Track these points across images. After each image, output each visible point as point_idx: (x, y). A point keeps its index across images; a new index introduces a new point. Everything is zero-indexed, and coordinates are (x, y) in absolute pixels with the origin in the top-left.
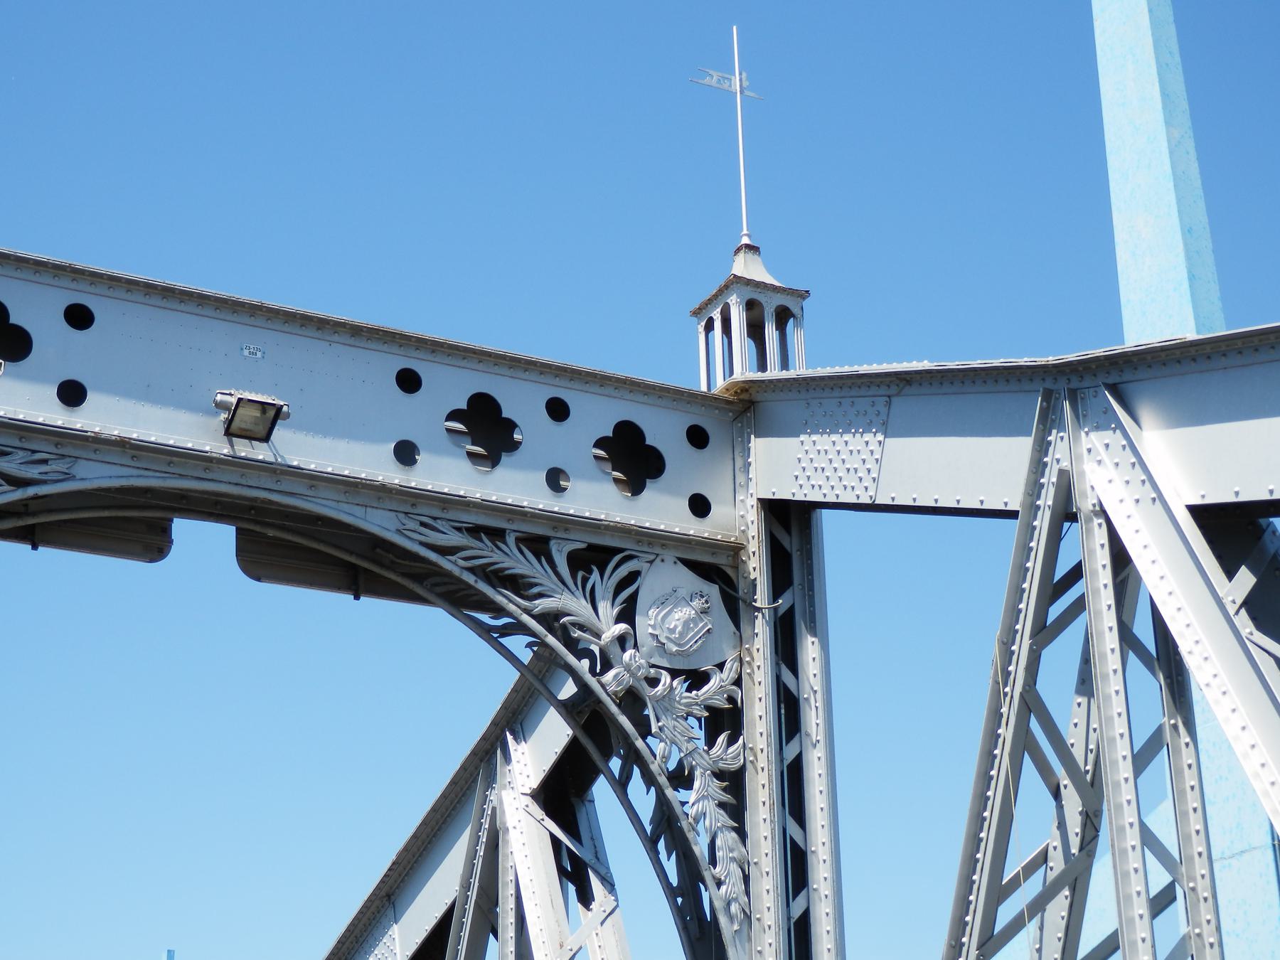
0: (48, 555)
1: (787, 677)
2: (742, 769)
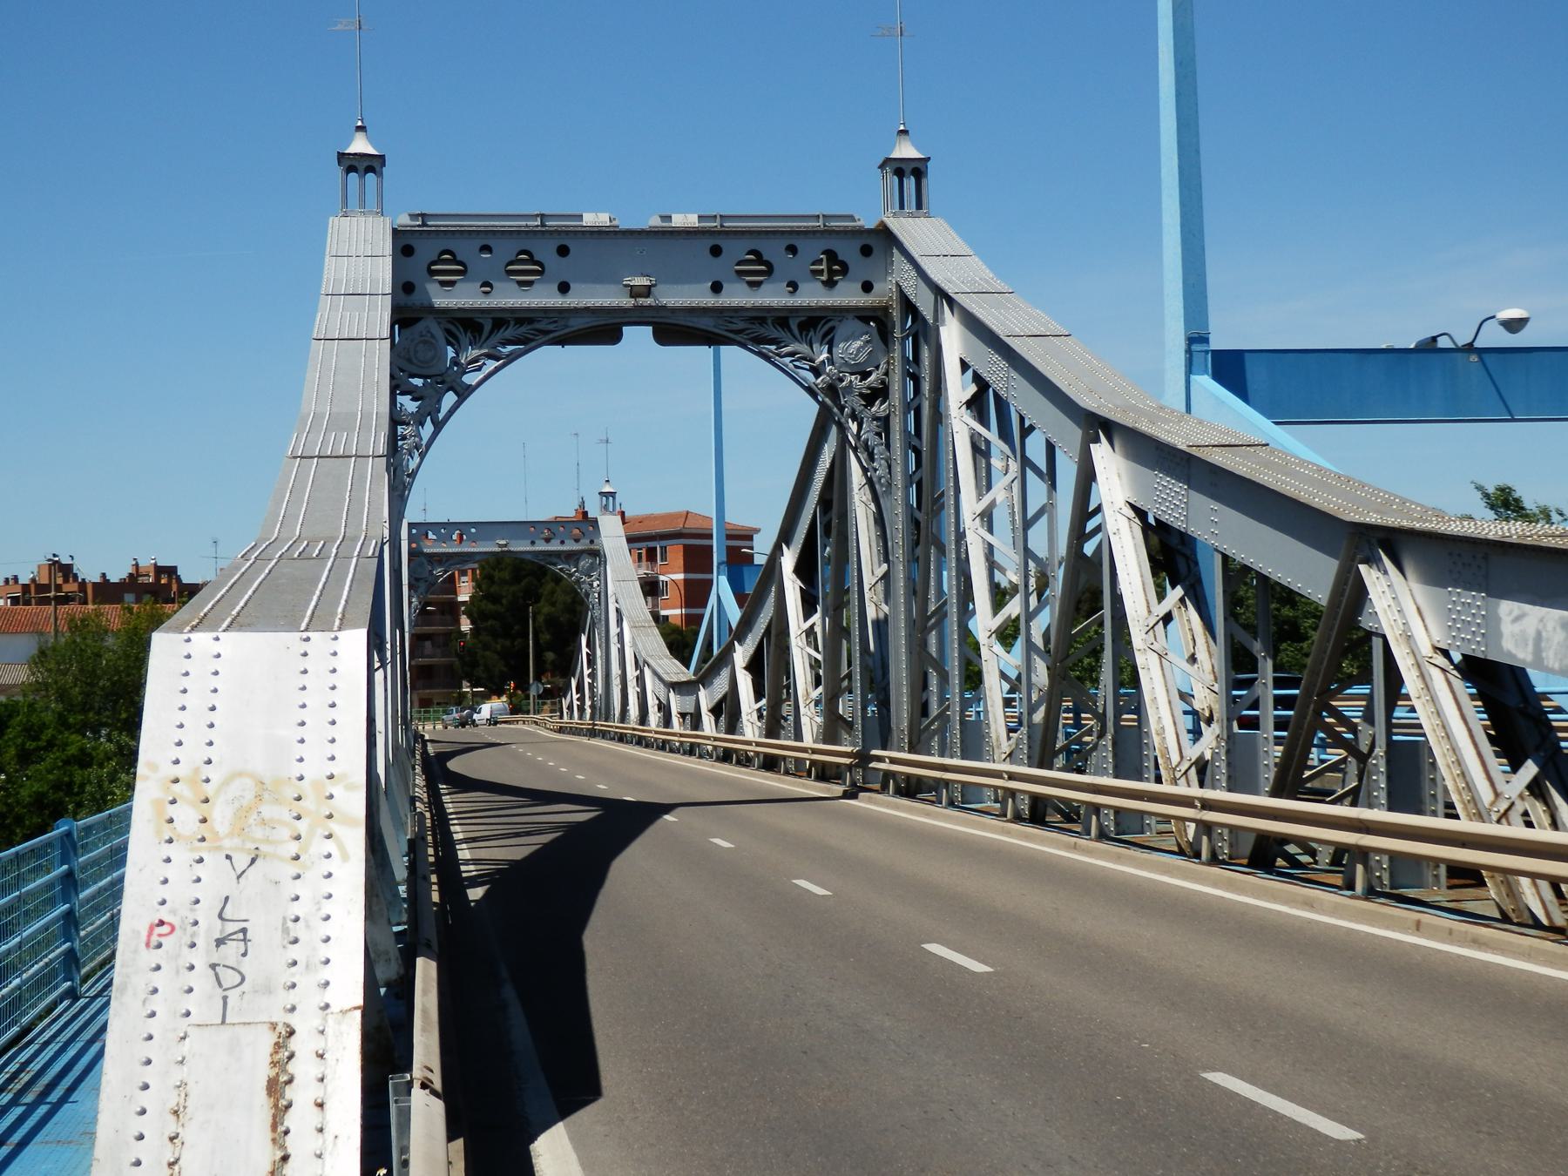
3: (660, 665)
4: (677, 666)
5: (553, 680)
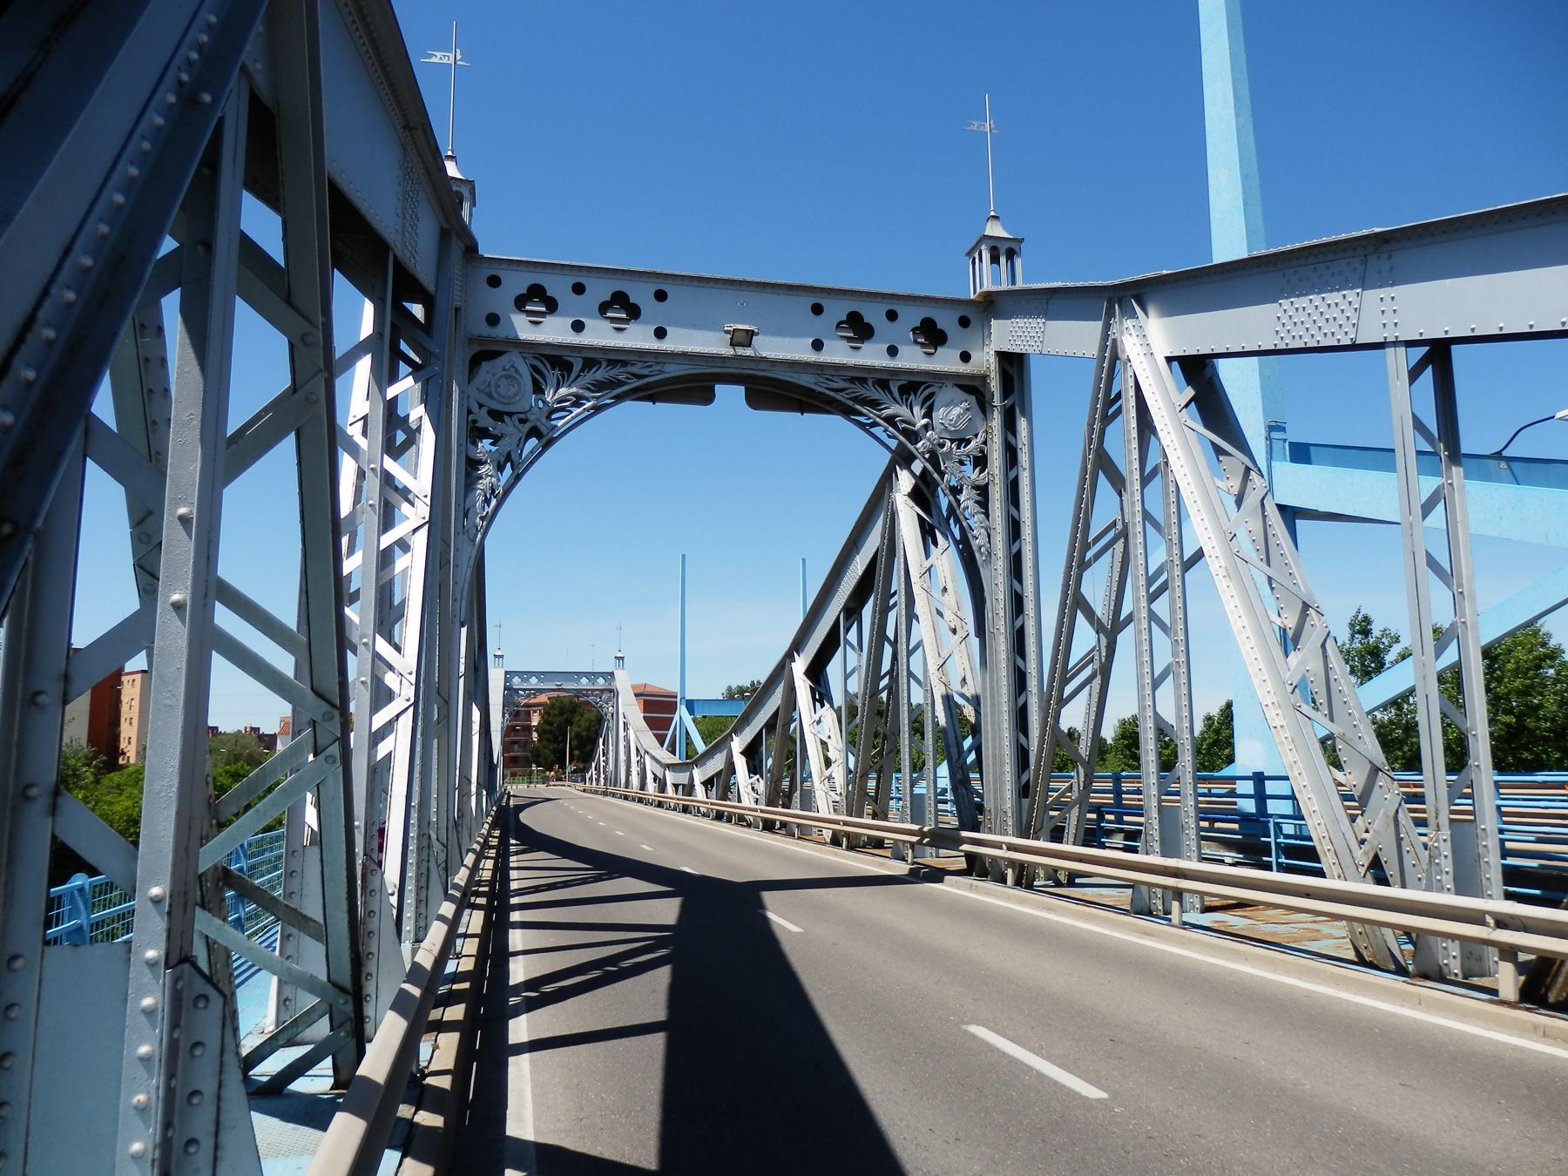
0: (661, 407)
1: (1011, 438)
2: (988, 484)
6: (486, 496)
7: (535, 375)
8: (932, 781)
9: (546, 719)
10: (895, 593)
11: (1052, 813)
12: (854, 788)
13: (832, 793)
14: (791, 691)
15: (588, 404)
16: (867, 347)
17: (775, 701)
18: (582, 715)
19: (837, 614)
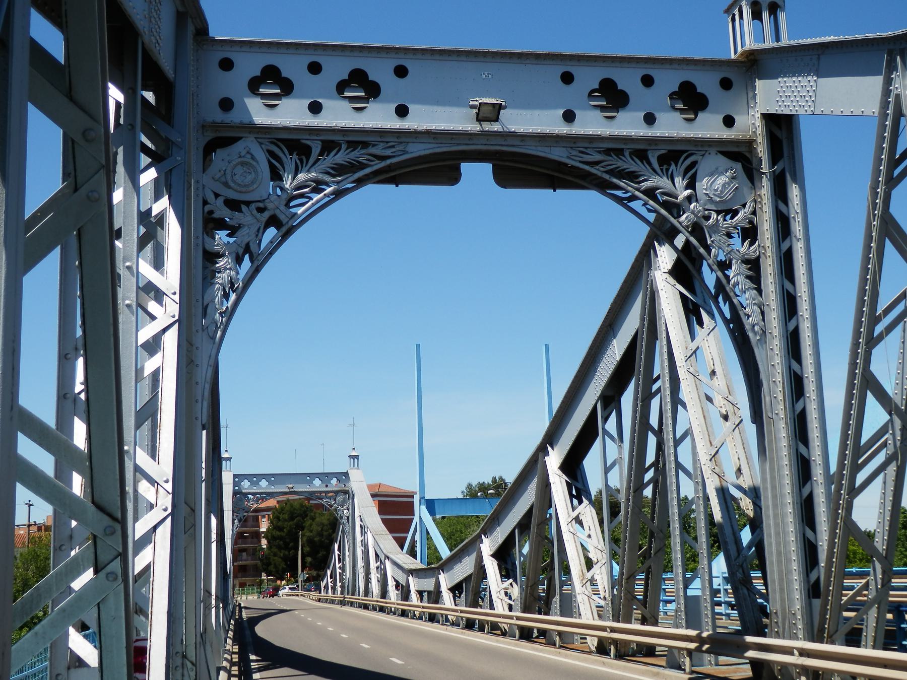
1: (782, 207)
2: (758, 258)
3: (397, 558)
4: (412, 560)
5: (310, 572)
6: (224, 290)
7: (270, 158)
8: (707, 582)
9: (275, 525)
10: (658, 377)
11: (846, 614)
12: (620, 592)
13: (595, 597)
14: (545, 488)
15: (329, 190)
16: (623, 116)
17: (528, 498)
18: (313, 519)
19: (594, 403)
